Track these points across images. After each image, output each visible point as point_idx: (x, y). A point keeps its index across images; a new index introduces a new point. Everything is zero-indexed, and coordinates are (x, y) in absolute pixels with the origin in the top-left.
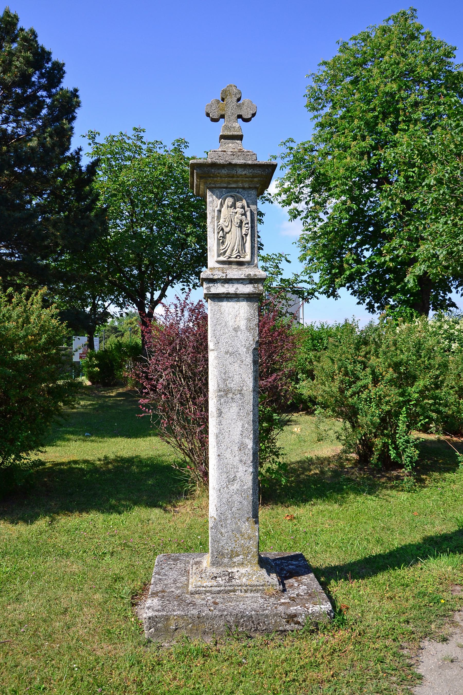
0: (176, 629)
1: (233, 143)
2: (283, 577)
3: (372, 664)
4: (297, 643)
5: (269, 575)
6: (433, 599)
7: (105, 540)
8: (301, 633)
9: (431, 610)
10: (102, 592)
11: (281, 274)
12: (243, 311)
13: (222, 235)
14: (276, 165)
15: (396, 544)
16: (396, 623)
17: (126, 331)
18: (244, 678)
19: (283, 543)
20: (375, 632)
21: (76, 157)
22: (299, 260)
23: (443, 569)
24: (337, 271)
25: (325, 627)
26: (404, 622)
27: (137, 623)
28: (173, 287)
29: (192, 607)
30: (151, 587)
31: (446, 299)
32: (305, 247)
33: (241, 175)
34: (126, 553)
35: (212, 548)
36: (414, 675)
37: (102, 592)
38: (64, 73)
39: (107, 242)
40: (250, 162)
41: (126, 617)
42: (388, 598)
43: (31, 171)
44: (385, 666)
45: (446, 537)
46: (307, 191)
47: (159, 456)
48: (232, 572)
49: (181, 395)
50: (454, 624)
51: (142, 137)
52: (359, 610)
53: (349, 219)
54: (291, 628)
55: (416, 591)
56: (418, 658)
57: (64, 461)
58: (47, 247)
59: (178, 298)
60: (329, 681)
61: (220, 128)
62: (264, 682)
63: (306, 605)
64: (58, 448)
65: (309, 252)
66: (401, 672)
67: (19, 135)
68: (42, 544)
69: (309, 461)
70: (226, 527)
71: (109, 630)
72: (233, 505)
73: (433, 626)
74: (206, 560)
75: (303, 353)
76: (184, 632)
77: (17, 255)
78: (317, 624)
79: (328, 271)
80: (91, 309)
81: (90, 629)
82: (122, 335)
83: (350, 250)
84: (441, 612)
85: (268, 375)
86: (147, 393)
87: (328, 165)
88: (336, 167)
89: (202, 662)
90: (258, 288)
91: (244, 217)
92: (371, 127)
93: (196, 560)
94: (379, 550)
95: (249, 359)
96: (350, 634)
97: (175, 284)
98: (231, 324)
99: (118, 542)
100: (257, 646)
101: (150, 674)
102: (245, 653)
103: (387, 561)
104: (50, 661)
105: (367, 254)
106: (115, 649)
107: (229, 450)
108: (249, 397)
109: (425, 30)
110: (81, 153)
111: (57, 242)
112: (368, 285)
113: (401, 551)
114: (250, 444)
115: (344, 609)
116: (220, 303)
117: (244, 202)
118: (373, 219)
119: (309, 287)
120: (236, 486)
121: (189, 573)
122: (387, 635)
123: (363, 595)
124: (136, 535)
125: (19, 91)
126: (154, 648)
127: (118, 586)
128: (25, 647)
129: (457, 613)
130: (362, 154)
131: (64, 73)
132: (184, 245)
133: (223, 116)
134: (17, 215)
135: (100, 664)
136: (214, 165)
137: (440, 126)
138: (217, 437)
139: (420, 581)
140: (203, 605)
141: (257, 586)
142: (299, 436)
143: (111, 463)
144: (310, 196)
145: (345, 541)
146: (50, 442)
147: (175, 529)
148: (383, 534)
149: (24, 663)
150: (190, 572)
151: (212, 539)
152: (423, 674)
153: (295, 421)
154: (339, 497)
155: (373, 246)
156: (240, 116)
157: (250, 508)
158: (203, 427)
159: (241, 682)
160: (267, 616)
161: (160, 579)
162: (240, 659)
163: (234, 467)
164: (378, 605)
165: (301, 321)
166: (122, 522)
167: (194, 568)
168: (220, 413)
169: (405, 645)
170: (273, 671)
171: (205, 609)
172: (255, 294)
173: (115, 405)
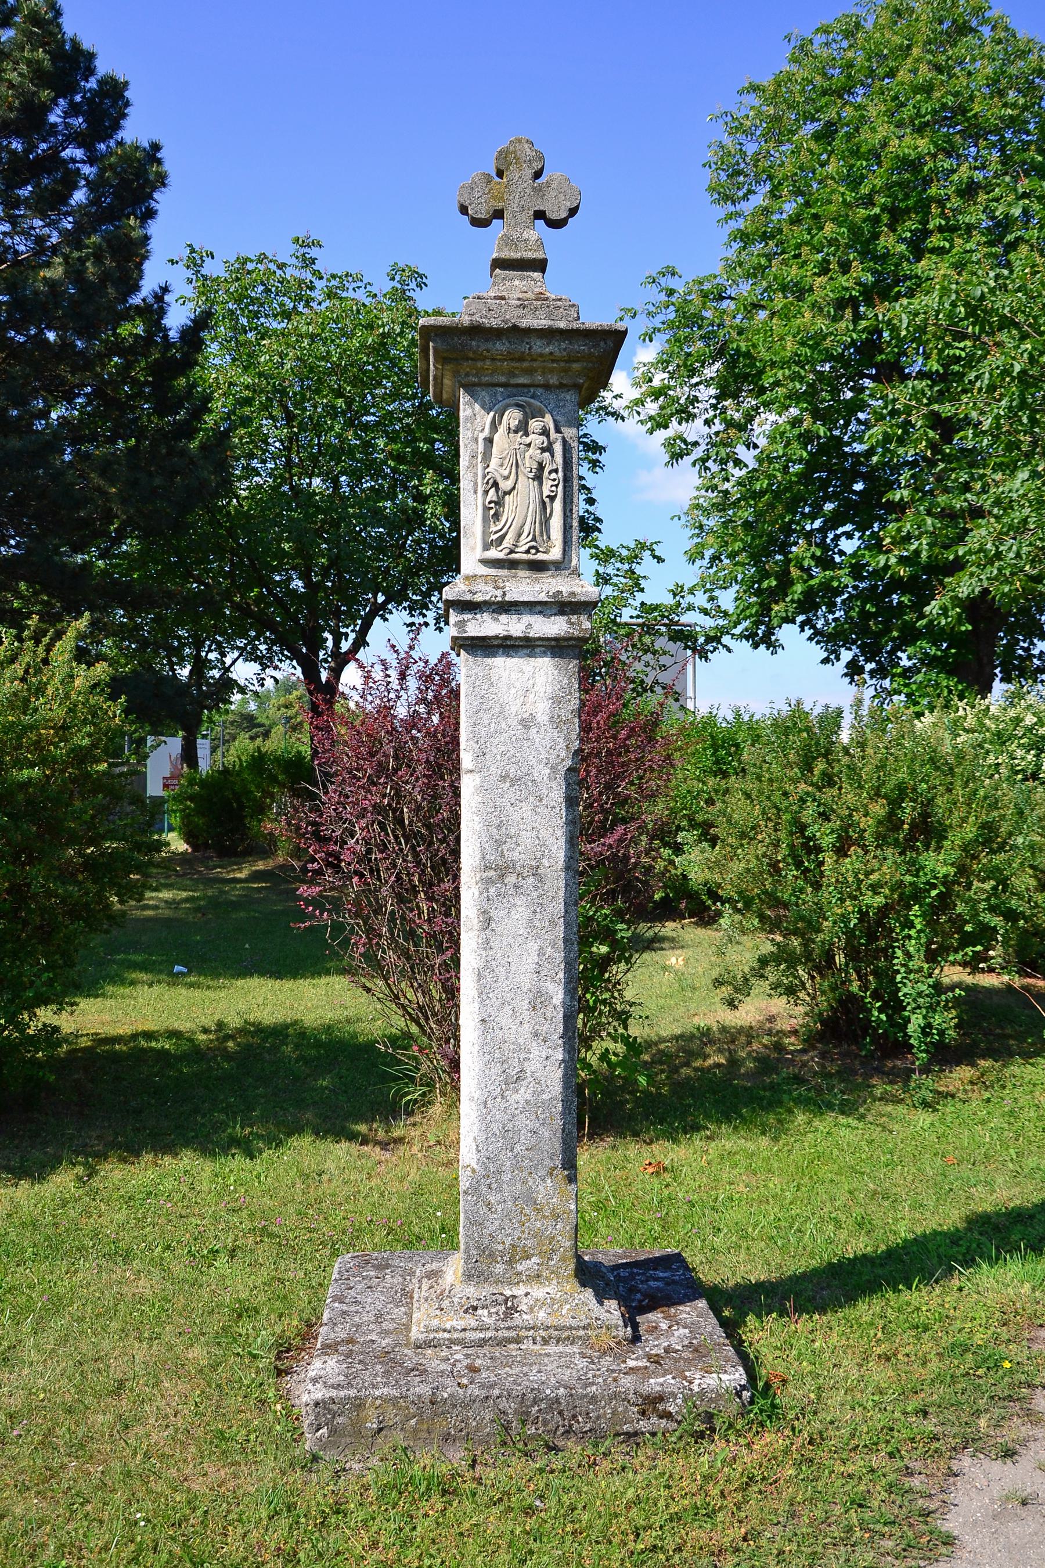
0: (381, 1430)
1: (522, 279)
2: (635, 1308)
3: (838, 1510)
4: (663, 1463)
5: (602, 1304)
6: (985, 1360)
7: (216, 1220)
8: (673, 1439)
9: (979, 1385)
10: (207, 1344)
11: (642, 590)
12: (544, 679)
13: (495, 499)
14: (625, 333)
15: (904, 1231)
16: (897, 1415)
17: (274, 724)
18: (538, 1544)
19: (638, 1227)
20: (847, 1436)
21: (154, 311)
22: (685, 558)
23: (1010, 1290)
24: (774, 583)
25: (731, 1426)
26: (916, 1413)
27: (288, 1416)
28: (386, 620)
29: (418, 1379)
30: (323, 1330)
31: (1034, 656)
32: (701, 527)
33: (541, 355)
34: (265, 1251)
35: (470, 1237)
36: (934, 1536)
37: (207, 1344)
38: (127, 104)
39: (229, 513)
40: (562, 325)
41: (263, 1402)
42: (879, 1356)
43: (47, 340)
44: (867, 1515)
45: (1019, 1215)
46: (707, 393)
47: (348, 1021)
48: (514, 1297)
49: (398, 878)
50: (1030, 1415)
51: (313, 261)
52: (810, 1384)
53: (807, 463)
54: (649, 1428)
55: (946, 1341)
56: (945, 1497)
57: (121, 1032)
58: (86, 523)
59: (393, 646)
60: (737, 1550)
61: (492, 242)
62: (585, 1553)
63: (687, 1374)
64: (110, 1002)
65: (711, 540)
66: (905, 1528)
67: (16, 253)
68: (67, 1230)
69: (703, 1034)
70: (500, 1189)
71: (222, 1433)
72: (516, 1139)
73: (983, 1422)
74: (453, 1268)
75: (688, 777)
76: (398, 1437)
77: (12, 542)
78: (709, 1417)
79: (751, 587)
80: (191, 671)
81: (177, 1430)
82: (266, 735)
83: (808, 535)
84: (1002, 1390)
85: (604, 830)
86: (319, 872)
87: (758, 332)
88: (777, 337)
89: (439, 1506)
90: (580, 624)
91: (547, 455)
92: (863, 242)
93: (428, 1267)
94: (862, 1246)
95: (557, 794)
96: (788, 1442)
97: (391, 613)
98: (514, 710)
99: (247, 1225)
100: (570, 1469)
101: (317, 1534)
102: (542, 1485)
103: (879, 1271)
104: (82, 1504)
105: (848, 546)
106: (235, 1476)
107: (507, 1009)
108: (557, 883)
109: (994, 14)
110: (167, 298)
111: (111, 509)
112: (848, 617)
113: (915, 1248)
114: (557, 994)
115: (776, 1383)
116: (489, 661)
117: (548, 420)
118: (862, 464)
119: (708, 622)
120: (523, 1094)
121: (412, 1298)
122: (876, 1444)
123: (822, 1351)
124: (291, 1209)
125: (16, 145)
126: (327, 1475)
127: (244, 1327)
128: (22, 1472)
129: (1038, 1391)
130: (841, 304)
131: (127, 104)
132: (414, 520)
133: (499, 214)
134: (15, 443)
135: (199, 1512)
136: (476, 331)
137: (1027, 241)
138: (480, 976)
139: (956, 1319)
140: (444, 1373)
141: (571, 1328)
142: (679, 976)
143: (232, 1037)
144: (714, 407)
145: (783, 1224)
146: (90, 988)
147: (382, 1195)
148: (872, 1208)
149: (18, 1511)
150: (416, 1296)
151: (467, 1218)
152: (956, 1533)
153: (672, 940)
154: (771, 1119)
155: (862, 527)
156: (539, 215)
157: (558, 1146)
158: (449, 953)
159: (531, 1552)
160: (593, 1399)
161: (344, 1312)
162: (529, 1501)
163: (519, 1048)
164: (855, 1374)
165: (690, 705)
166: (258, 1177)
167: (425, 1287)
168: (487, 921)
169: (917, 1466)
170: (607, 1526)
171: (449, 1382)
172: (571, 639)
173: (246, 902)
